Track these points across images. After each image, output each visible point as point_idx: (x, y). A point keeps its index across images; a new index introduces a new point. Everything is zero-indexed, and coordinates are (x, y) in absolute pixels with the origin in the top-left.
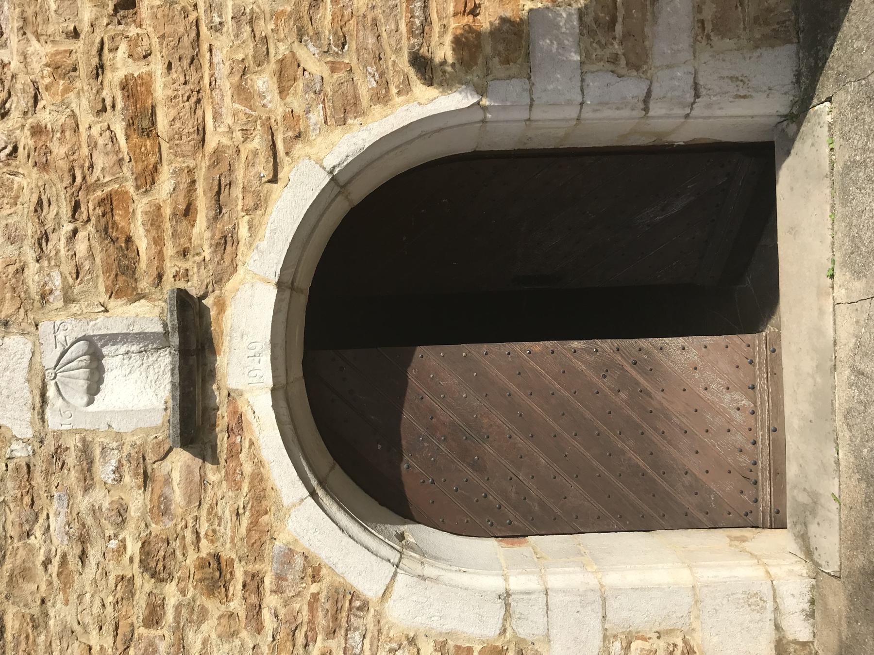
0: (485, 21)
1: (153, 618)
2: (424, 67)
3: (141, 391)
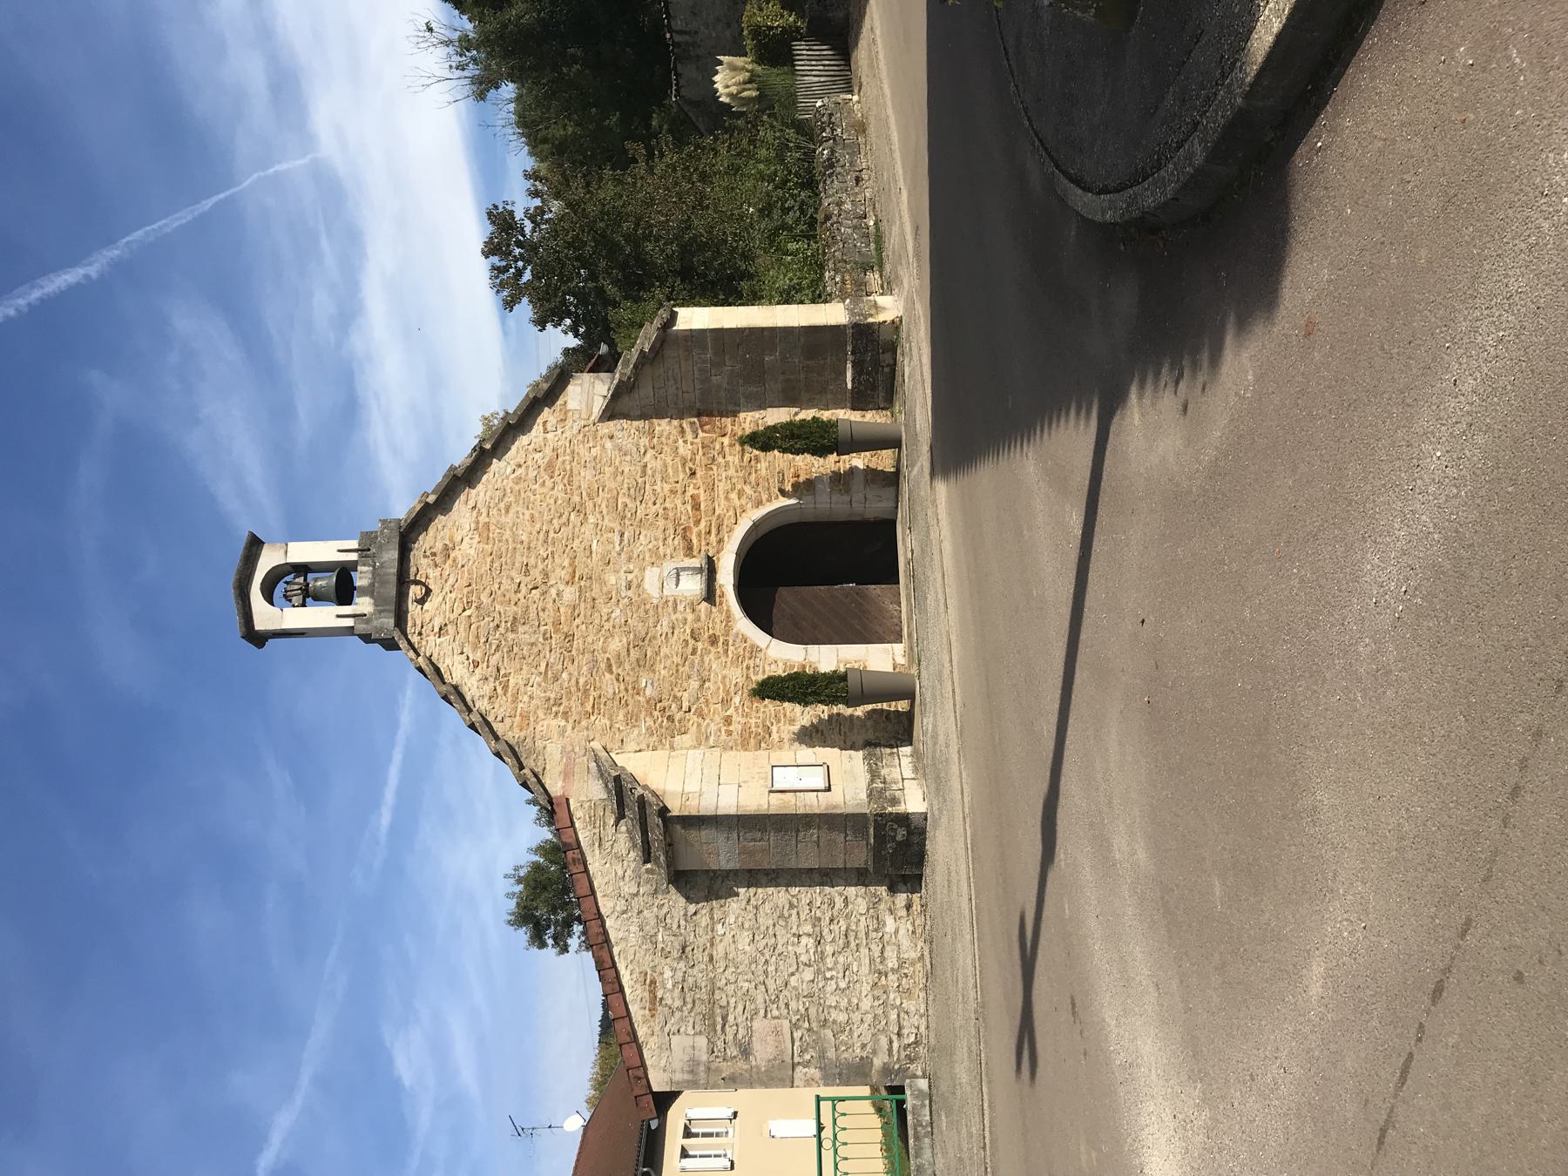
0: (801, 479)
1: (694, 652)
2: (783, 492)
3: (693, 586)
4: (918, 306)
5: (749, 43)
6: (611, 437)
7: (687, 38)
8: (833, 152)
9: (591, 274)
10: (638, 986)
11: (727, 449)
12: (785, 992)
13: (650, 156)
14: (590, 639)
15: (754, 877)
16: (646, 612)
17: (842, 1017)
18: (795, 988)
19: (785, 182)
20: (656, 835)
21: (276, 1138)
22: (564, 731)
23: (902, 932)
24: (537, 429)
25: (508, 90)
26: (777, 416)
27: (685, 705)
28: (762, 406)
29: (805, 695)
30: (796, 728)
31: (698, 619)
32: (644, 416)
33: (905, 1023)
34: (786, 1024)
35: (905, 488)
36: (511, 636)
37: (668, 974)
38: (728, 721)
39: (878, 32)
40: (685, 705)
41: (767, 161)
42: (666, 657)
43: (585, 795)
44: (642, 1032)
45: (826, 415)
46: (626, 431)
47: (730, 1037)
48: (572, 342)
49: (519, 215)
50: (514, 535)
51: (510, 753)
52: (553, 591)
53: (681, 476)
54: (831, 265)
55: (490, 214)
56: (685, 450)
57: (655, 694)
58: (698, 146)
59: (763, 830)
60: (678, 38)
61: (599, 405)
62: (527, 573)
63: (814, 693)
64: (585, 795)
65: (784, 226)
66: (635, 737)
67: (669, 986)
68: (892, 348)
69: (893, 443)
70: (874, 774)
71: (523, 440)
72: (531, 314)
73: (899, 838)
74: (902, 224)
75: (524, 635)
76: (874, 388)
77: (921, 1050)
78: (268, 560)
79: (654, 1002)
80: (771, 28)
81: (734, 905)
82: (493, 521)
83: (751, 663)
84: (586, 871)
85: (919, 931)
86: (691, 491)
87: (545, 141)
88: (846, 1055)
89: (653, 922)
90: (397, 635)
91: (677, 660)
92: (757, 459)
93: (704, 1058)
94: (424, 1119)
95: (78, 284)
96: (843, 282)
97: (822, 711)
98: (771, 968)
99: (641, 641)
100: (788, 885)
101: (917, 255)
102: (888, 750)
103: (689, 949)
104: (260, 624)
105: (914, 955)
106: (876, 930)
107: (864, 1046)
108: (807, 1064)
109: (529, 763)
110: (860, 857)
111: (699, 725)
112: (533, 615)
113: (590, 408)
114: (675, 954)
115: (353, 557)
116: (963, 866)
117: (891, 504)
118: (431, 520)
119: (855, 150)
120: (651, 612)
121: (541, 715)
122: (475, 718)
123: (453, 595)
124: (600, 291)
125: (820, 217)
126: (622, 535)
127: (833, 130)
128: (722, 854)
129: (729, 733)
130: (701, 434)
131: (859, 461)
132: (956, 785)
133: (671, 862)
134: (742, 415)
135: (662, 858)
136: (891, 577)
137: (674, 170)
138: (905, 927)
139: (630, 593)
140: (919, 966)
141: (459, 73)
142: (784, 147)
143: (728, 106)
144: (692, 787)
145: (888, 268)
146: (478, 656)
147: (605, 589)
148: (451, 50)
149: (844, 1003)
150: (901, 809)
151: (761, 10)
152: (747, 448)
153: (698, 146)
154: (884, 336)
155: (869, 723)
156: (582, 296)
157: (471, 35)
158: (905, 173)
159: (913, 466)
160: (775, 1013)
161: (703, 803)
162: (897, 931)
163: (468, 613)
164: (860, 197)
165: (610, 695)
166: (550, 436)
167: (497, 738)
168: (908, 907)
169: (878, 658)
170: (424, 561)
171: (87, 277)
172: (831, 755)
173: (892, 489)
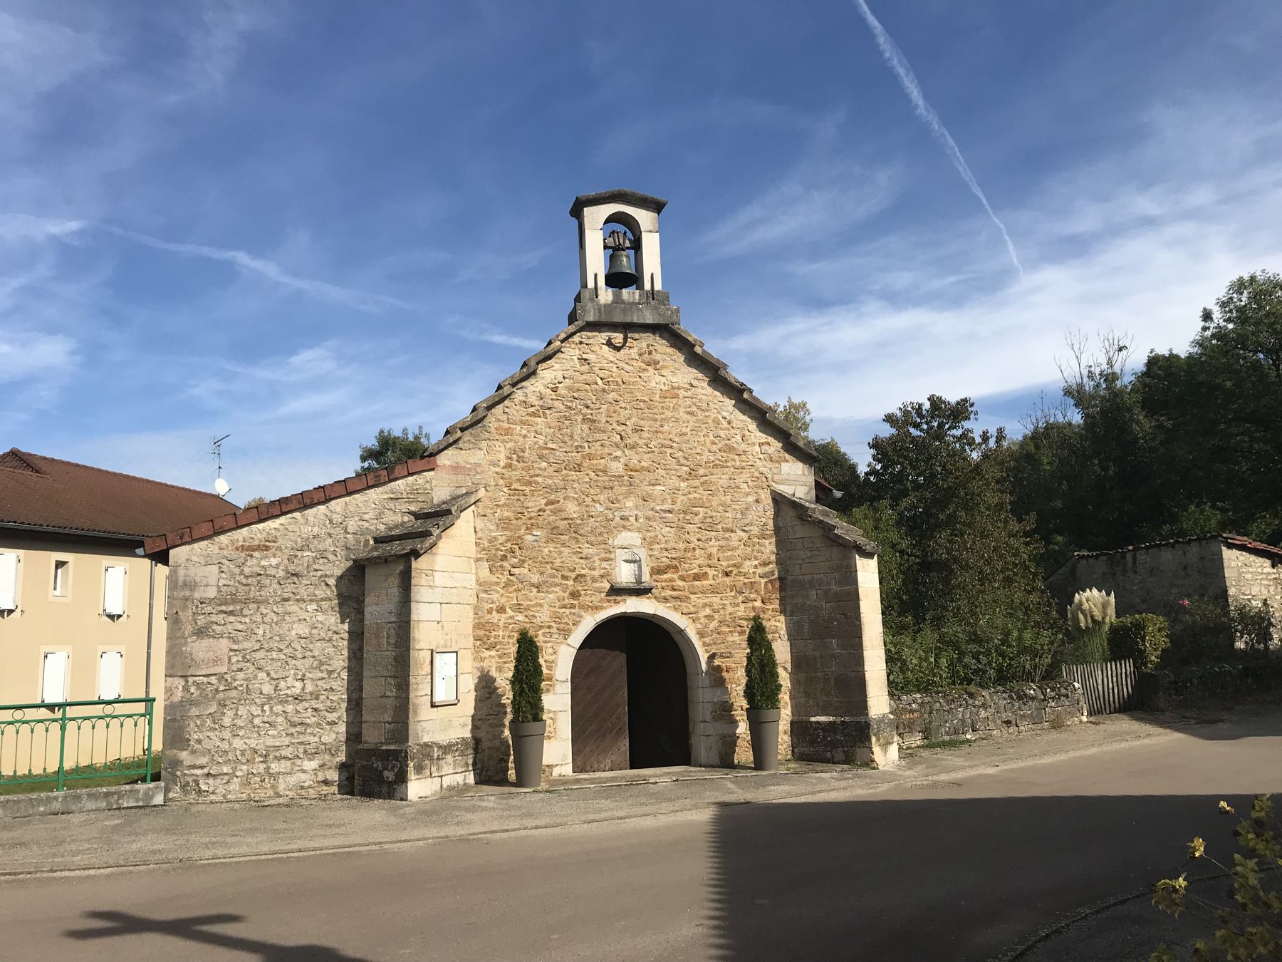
0: (724, 674)
1: (564, 577)
3: (625, 575)
4: (886, 786)
5: (1128, 620)
6: (757, 501)
7: (1130, 564)
8: (1033, 699)
9: (915, 486)
10: (264, 535)
11: (750, 605)
12: (252, 668)
13: (1026, 534)
14: (576, 485)
15: (357, 637)
16: (601, 534)
17: (227, 721)
18: (256, 676)
19: (1002, 655)
20: (396, 548)
21: (257, 264)
22: (495, 465)
23: (303, 776)
24: (763, 437)
25: (1077, 418)
26: (782, 651)
27: (516, 571)
28: (791, 637)
29: (521, 682)
30: (494, 673)
31: (594, 580)
32: (777, 529)
33: (218, 781)
34: (223, 669)
35: (716, 775)
36: (579, 418)
37: (274, 561)
38: (501, 610)
39: (1147, 741)
40: (516, 571)
41: (1020, 639)
42: (560, 553)
43: (437, 485)
44: (223, 539)
45: (785, 697)
46: (763, 515)
47: (214, 618)
48: (862, 469)
49: (967, 425)
50: (667, 420)
51: (476, 421)
52: (619, 453)
53: (725, 564)
54: (926, 699)
55: (965, 400)
56: (748, 566)
57: (527, 543)
58: (1035, 575)
59: (397, 646)
60: (1129, 557)
61: (786, 490)
62: (635, 431)
63: (522, 690)
64: (437, 485)
65: (962, 654)
66: (489, 527)
67: (263, 563)
68: (849, 760)
69: (759, 764)
70: (447, 749)
71: (752, 426)
72: (882, 436)
73: (386, 773)
74: (964, 767)
75: (581, 429)
76: (812, 743)
77: (192, 797)
78: (644, 218)
79: (249, 549)
80: (1143, 639)
81: (333, 619)
82: (680, 402)
83: (554, 630)
84: (369, 487)
85: (303, 793)
86: (711, 572)
87: (1037, 447)
88: (192, 725)
89: (321, 547)
90: (580, 323)
91: (558, 563)
92: (741, 633)
93: (197, 595)
94: (264, 373)
95: (911, 101)
96: (912, 711)
97: (507, 698)
98: (274, 655)
99: (574, 530)
100: (350, 669)
101: (934, 785)
102: (470, 761)
103: (295, 579)
104: (587, 211)
105: (281, 788)
106: (305, 752)
107: (199, 741)
108: (186, 689)
109: (467, 436)
110: (372, 736)
111: (497, 584)
112: (597, 436)
113: (782, 482)
114: (291, 568)
115: (647, 286)
116: (336, 842)
117: (703, 761)
118: (680, 350)
119: (1036, 720)
120: (600, 538)
121: (509, 445)
122: (507, 390)
123: (615, 369)
124: (905, 493)
125: (972, 688)
126: (669, 511)
127: (1053, 698)
128: (378, 608)
129: (490, 611)
130: (763, 581)
131: (743, 729)
132: (416, 834)
133: (372, 561)
134: (782, 618)
135: (376, 554)
136: (636, 761)
137: (1014, 555)
138: (307, 779)
139: (617, 519)
140: (271, 793)
141: (1085, 373)
142: (1035, 654)
143: (1071, 602)
144: (439, 579)
145: (926, 753)
146: (562, 391)
147: (621, 497)
148: (1105, 366)
149: (239, 722)
150: (412, 775)
151: (1159, 630)
152: (751, 624)
153: (1035, 575)
154: (860, 752)
155: (497, 743)
156: (901, 477)
157: (1119, 383)
158: (1012, 771)
159: (736, 783)
160: (234, 659)
161: (423, 589)
162: (304, 771)
163: (600, 382)
164: (992, 726)
165: (526, 504)
166: (757, 448)
167: (489, 408)
168: (326, 782)
169: (557, 750)
170: (644, 345)
171: (917, 106)
172: (468, 706)
173: (717, 761)
